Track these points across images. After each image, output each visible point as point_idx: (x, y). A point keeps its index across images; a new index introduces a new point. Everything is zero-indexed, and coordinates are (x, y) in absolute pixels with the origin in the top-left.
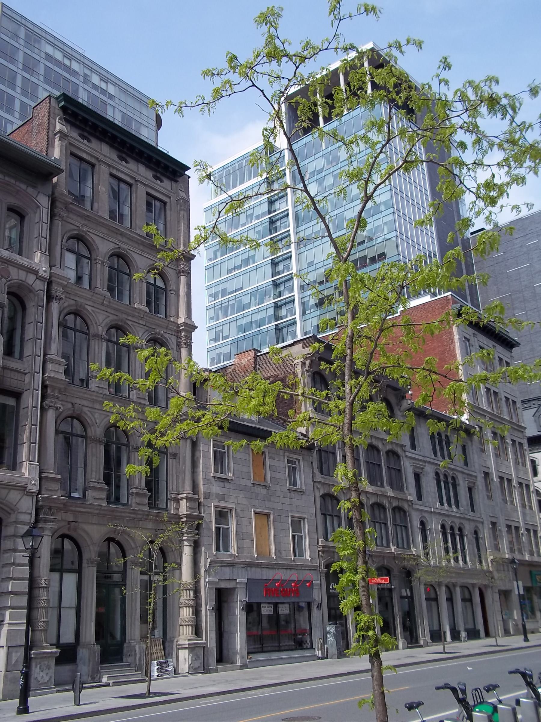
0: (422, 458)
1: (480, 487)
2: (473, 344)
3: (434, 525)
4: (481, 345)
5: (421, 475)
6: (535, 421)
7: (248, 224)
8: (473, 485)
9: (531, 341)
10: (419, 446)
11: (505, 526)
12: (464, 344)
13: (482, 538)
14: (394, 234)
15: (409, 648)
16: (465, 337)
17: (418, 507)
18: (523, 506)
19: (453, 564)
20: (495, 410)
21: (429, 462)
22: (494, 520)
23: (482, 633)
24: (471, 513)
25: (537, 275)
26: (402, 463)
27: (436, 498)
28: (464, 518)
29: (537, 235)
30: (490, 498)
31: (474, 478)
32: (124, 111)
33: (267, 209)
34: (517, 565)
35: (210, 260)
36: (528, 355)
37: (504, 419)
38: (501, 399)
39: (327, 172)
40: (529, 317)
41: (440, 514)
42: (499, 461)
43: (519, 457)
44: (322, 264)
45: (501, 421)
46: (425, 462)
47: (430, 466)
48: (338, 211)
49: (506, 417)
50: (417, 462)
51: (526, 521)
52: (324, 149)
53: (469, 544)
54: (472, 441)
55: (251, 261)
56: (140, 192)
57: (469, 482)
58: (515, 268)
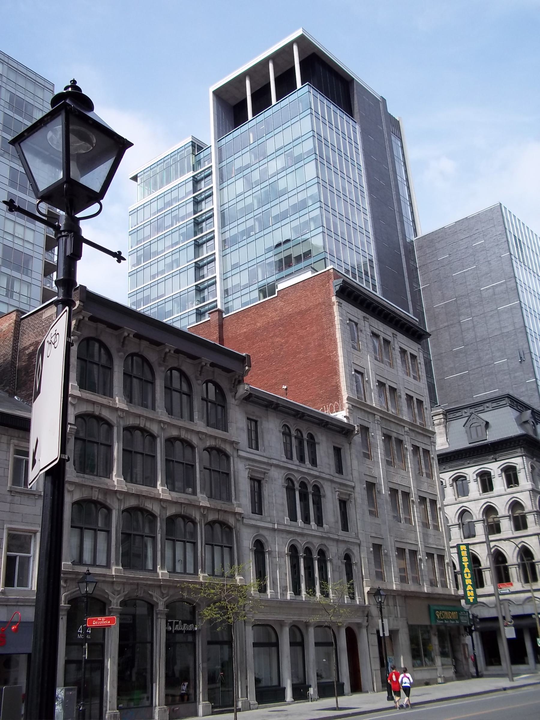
0: (265, 460)
1: (359, 501)
2: (363, 328)
3: (278, 547)
4: (375, 331)
6: (466, 432)
7: (172, 225)
8: (347, 498)
9: (477, 350)
10: (263, 445)
11: (425, 554)
12: (348, 328)
13: (356, 564)
14: (320, 229)
15: (213, 713)
16: (350, 320)
17: (253, 522)
18: (425, 525)
19: (304, 596)
21: (277, 466)
22: (377, 542)
23: (347, 687)
24: (341, 533)
25: (483, 278)
26: (232, 465)
27: (283, 511)
28: (329, 539)
29: (484, 235)
30: (373, 513)
31: (352, 490)
32: (13, 91)
33: (192, 210)
34: (383, 597)
35: (134, 266)
38: (400, 397)
39: (253, 168)
40: (475, 323)
41: (289, 532)
42: (392, 469)
43: (423, 466)
44: (246, 266)
45: (399, 422)
46: (271, 465)
47: (279, 470)
48: (264, 208)
51: (428, 544)
52: (252, 143)
53: (333, 571)
54: (350, 444)
55: (175, 265)
57: (341, 493)
58: (460, 271)
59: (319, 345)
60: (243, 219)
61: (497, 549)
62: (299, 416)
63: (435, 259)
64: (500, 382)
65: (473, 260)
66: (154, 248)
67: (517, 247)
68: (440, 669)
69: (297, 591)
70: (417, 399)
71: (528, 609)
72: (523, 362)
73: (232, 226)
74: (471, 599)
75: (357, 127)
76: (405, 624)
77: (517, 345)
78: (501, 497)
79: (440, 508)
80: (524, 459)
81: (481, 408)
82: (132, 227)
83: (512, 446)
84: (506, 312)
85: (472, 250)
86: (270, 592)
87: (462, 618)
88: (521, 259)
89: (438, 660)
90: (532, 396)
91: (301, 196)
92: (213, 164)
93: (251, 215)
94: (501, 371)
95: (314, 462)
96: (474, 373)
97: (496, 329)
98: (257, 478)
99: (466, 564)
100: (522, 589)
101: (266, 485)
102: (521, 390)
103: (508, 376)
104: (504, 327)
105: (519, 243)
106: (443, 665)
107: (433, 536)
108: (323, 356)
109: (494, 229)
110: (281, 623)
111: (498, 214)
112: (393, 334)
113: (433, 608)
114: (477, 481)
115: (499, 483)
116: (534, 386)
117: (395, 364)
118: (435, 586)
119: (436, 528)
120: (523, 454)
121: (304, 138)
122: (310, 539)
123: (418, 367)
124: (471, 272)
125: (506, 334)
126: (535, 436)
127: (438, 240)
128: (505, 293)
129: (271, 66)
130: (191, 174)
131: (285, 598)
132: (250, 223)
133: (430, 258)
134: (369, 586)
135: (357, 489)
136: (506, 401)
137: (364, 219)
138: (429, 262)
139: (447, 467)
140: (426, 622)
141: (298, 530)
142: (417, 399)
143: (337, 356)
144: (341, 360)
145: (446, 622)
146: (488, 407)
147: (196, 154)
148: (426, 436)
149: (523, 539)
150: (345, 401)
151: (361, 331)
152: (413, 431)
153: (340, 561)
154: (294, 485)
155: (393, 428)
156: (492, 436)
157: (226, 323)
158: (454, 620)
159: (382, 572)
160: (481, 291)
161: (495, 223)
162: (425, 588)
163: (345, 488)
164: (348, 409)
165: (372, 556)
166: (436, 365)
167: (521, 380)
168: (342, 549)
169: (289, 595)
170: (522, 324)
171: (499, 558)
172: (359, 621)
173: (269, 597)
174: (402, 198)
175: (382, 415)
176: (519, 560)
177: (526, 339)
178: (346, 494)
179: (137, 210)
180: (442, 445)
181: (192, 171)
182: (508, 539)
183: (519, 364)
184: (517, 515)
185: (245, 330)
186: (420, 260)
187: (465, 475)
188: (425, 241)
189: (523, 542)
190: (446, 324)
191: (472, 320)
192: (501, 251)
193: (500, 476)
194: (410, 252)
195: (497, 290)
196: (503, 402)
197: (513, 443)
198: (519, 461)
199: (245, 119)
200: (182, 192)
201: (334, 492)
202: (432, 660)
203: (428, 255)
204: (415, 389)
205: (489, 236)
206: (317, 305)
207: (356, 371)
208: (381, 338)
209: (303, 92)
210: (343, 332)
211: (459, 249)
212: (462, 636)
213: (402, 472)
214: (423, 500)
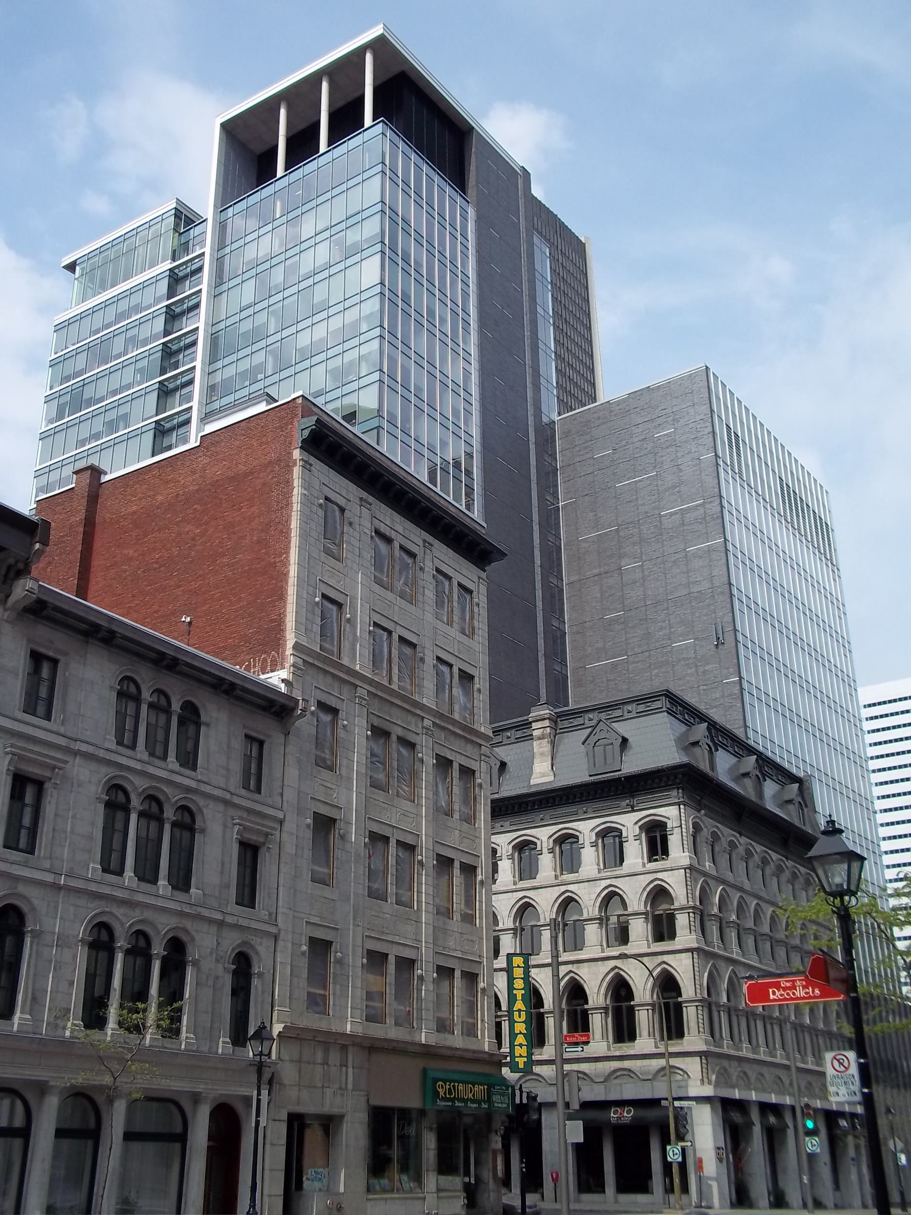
0: (62, 741)
1: (289, 848)
2: (356, 520)
4: (383, 529)
5: (48, 785)
8: (262, 840)
9: (646, 620)
10: (64, 711)
12: (321, 513)
18: (444, 912)
20: (395, 678)
22: (320, 934)
25: (667, 493)
29: (674, 420)
35: (51, 421)
36: (640, 646)
37: (423, 707)
40: (646, 573)
42: (380, 795)
45: (413, 708)
46: (76, 753)
47: (93, 766)
49: (429, 701)
50: (31, 747)
55: (122, 424)
58: (629, 479)
59: (259, 542)
60: (248, 351)
61: (618, 975)
62: (164, 663)
63: (589, 456)
64: (680, 679)
66: (88, 393)
68: (431, 1199)
69: (94, 1016)
70: (460, 669)
71: (659, 1090)
72: (720, 647)
73: (227, 361)
74: (521, 1062)
75: (471, 212)
76: (363, 1105)
77: (713, 615)
78: (635, 877)
79: (482, 882)
80: (682, 811)
81: (618, 713)
82: (56, 353)
84: (701, 557)
85: (652, 445)
86: (20, 1019)
87: (495, 1098)
89: (431, 1180)
90: (731, 707)
91: (351, 316)
92: (207, 250)
93: (262, 344)
94: (683, 659)
95: (189, 760)
96: (636, 660)
98: (36, 778)
99: (519, 994)
100: (654, 1051)
101: (55, 792)
102: (714, 696)
103: (693, 670)
105: (735, 440)
106: (439, 1190)
107: (458, 935)
108: (263, 563)
109: (692, 411)
110: (196, 1099)
111: (701, 384)
112: (425, 541)
113: (432, 1074)
115: (635, 852)
116: (736, 690)
117: (420, 597)
118: (449, 1032)
119: (469, 919)
120: (682, 800)
121: (366, 214)
122: (148, 915)
123: (472, 611)
126: (710, 773)
127: (597, 423)
128: (701, 523)
129: (325, 86)
130: (168, 265)
131: (59, 1032)
132: (259, 358)
134: (282, 1022)
135: (289, 826)
136: (663, 703)
137: (464, 367)
138: (578, 460)
140: (413, 1101)
141: (119, 894)
142: (460, 669)
143: (286, 563)
144: (293, 570)
145: (457, 1104)
146: (629, 712)
147: (182, 231)
148: (472, 742)
149: (666, 958)
150: (289, 651)
151: (351, 524)
153: (220, 966)
154: (128, 800)
155: (397, 717)
156: (632, 764)
157: (104, 493)
158: (479, 1102)
159: (325, 996)
160: (661, 516)
161: (696, 400)
162: (349, 1026)
163: (258, 820)
164: (293, 666)
165: (304, 963)
166: (573, 641)
168: (231, 942)
169: (72, 1026)
170: (726, 579)
171: (620, 989)
172: (244, 1091)
173: (15, 1028)
174: (541, 345)
175: (372, 689)
176: (655, 996)
177: (729, 606)
178: (258, 832)
179: (69, 323)
180: (543, 775)
181: (169, 261)
182: (636, 956)
183: (714, 649)
184: (661, 912)
185: (135, 508)
186: (563, 455)
187: (577, 834)
190: (596, 571)
191: (642, 566)
192: (701, 448)
193: (637, 838)
194: (547, 440)
195: (689, 517)
196: (658, 704)
197: (665, 779)
198: (672, 813)
200: (149, 296)
201: (230, 825)
202: (418, 1179)
203: (577, 448)
204: (459, 652)
206: (266, 466)
207: (324, 596)
208: (396, 545)
209: (374, 136)
210: (305, 519)
212: (493, 1134)
213: (406, 805)
214: (444, 863)
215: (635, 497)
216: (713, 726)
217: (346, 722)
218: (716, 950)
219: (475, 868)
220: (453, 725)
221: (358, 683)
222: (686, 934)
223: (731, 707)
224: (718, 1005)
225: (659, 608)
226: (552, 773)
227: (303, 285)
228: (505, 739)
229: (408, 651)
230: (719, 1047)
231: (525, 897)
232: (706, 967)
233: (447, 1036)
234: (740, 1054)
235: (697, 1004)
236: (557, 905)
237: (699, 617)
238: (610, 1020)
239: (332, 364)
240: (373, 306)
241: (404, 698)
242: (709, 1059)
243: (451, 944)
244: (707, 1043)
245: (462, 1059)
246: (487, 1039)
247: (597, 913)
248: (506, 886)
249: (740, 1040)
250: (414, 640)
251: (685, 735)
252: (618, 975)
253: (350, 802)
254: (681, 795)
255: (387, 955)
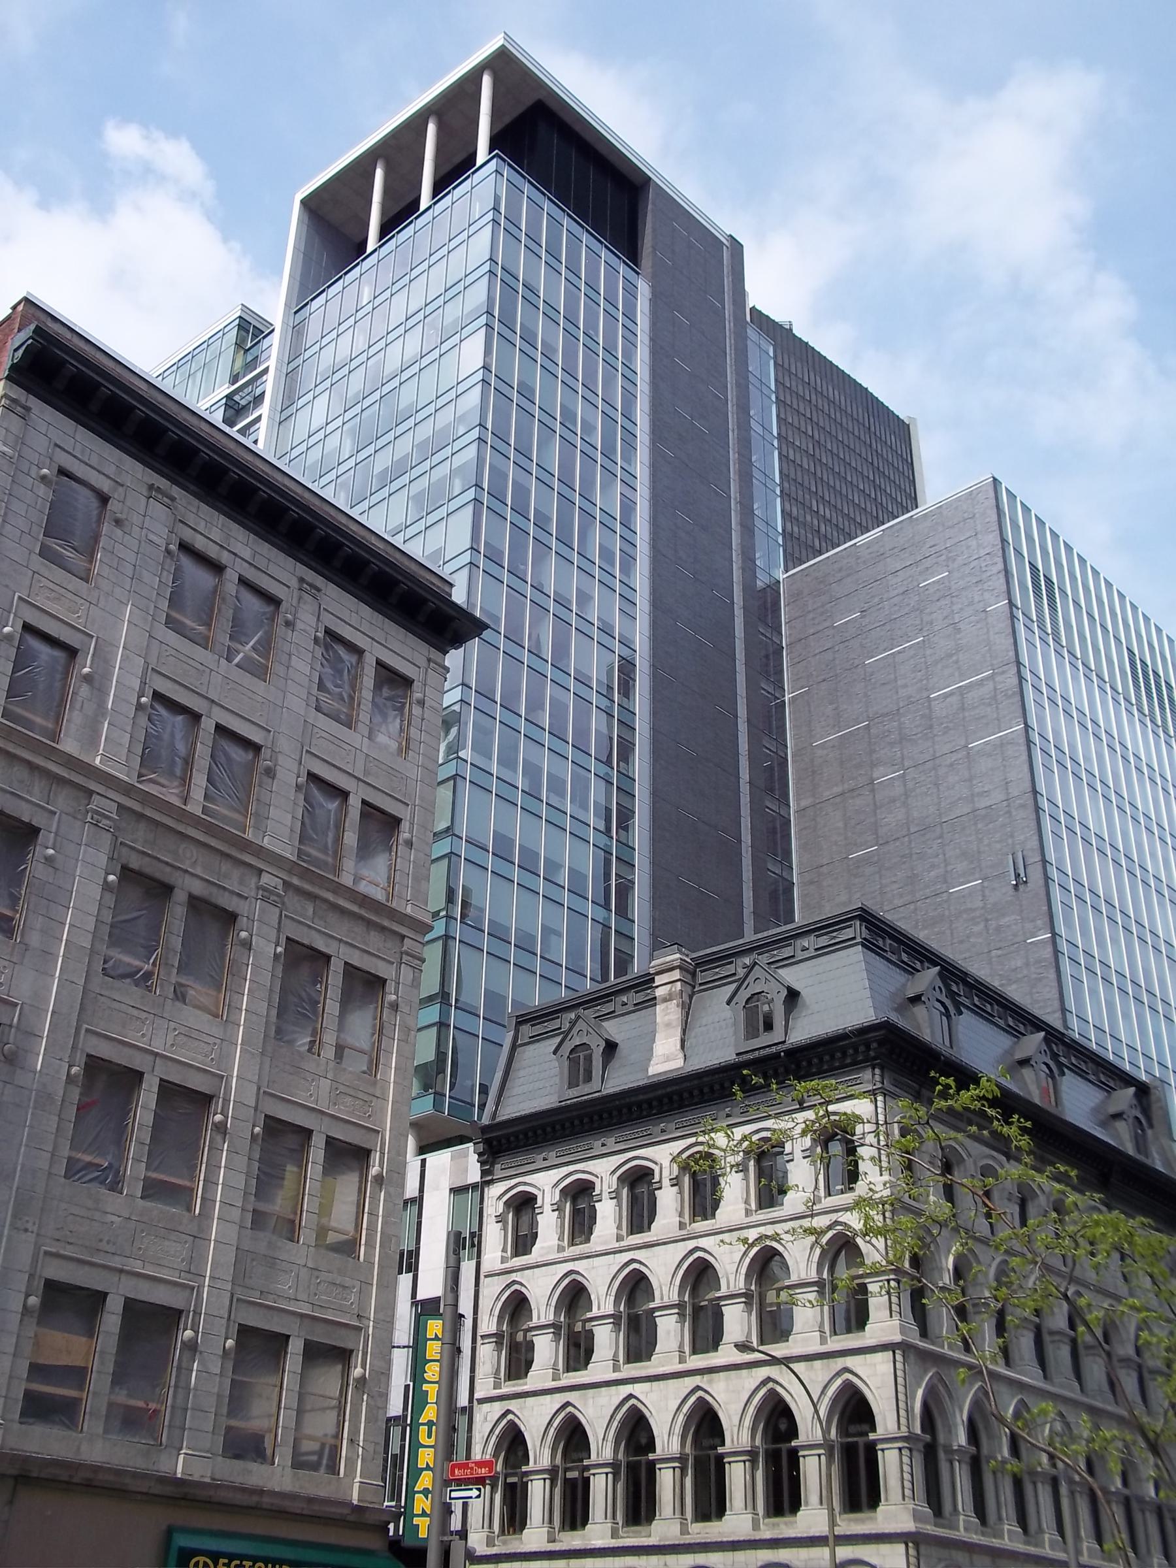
20: (198, 794)
25: (939, 666)
29: (948, 558)
37: (259, 851)
40: (910, 785)
45: (240, 852)
56: (308, 622)
58: (885, 650)
64: (961, 942)
65: (918, 622)
67: (1038, 594)
70: (364, 802)
72: (1021, 887)
75: (643, 288)
77: (1010, 841)
80: (880, 1104)
83: (848, 1061)
85: (917, 598)
88: (1146, 707)
90: (1040, 980)
97: (959, 799)
103: (982, 926)
104: (981, 794)
109: (973, 543)
114: (745, 1170)
116: (1048, 952)
120: (879, 1085)
124: (912, 652)
125: (983, 812)
127: (839, 576)
128: (990, 705)
130: (226, 390)
133: (816, 622)
136: (856, 930)
138: (812, 631)
139: (672, 1126)
142: (364, 802)
146: (804, 949)
148: (383, 929)
152: (299, 891)
156: (806, 1029)
161: (979, 528)
166: (803, 897)
167: (1015, 935)
170: (1027, 785)
171: (776, 1417)
177: (1033, 824)
180: (668, 1059)
183: (1011, 891)
186: (790, 628)
188: (809, 579)
189: (846, 1370)
190: (838, 790)
192: (987, 595)
196: (848, 933)
199: (359, 249)
205: (960, 561)
207: (27, 628)
209: (489, 179)
211: (885, 596)
215: (892, 676)
216: (951, 974)
217: (51, 851)
218: (946, 1350)
219: (367, 1153)
220: (334, 892)
221: (93, 786)
222: (885, 1322)
223: (1040, 980)
224: (1141, 1500)
225: (927, 836)
226: (681, 1055)
227: (386, 389)
228: (619, 1006)
229: (238, 754)
230: (1036, 1546)
231: (633, 1261)
232: (922, 1379)
233: (254, 1466)
234: (996, 1542)
235: (900, 1445)
236: (681, 1272)
237: (989, 845)
238: (760, 1475)
239: (416, 488)
240: (473, 398)
241: (210, 829)
242: (922, 1548)
243: (285, 1285)
244: (917, 1517)
245: (280, 1514)
246: (358, 1479)
247: (742, 1284)
248: (606, 1243)
249: (1000, 1518)
250: (256, 736)
251: (1009, 1052)
252: (772, 1392)
253: (40, 996)
254: (877, 1078)
255: (105, 1295)
